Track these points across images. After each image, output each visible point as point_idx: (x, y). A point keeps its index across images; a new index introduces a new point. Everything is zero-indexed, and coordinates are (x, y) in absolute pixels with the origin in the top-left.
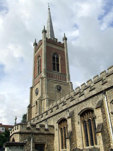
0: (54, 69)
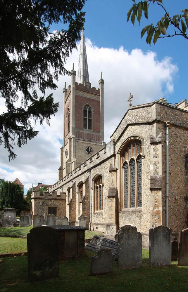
0: (85, 127)
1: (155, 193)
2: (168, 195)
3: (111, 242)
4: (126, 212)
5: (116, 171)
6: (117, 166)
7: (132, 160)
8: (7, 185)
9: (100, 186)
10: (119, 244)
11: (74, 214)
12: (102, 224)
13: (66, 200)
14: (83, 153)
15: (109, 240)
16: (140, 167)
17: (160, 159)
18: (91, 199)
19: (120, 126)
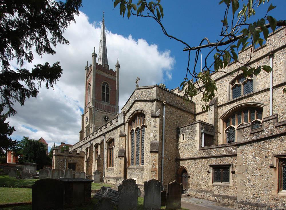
0: (103, 100)
1: (153, 154)
2: (163, 157)
3: (115, 192)
4: (132, 168)
5: (125, 136)
6: (126, 132)
7: (138, 128)
8: (30, 142)
9: (112, 147)
10: (119, 194)
11: (91, 170)
12: (113, 178)
13: (84, 158)
14: (101, 121)
15: (114, 190)
16: (143, 134)
17: (158, 129)
18: (105, 158)
19: (129, 101)
